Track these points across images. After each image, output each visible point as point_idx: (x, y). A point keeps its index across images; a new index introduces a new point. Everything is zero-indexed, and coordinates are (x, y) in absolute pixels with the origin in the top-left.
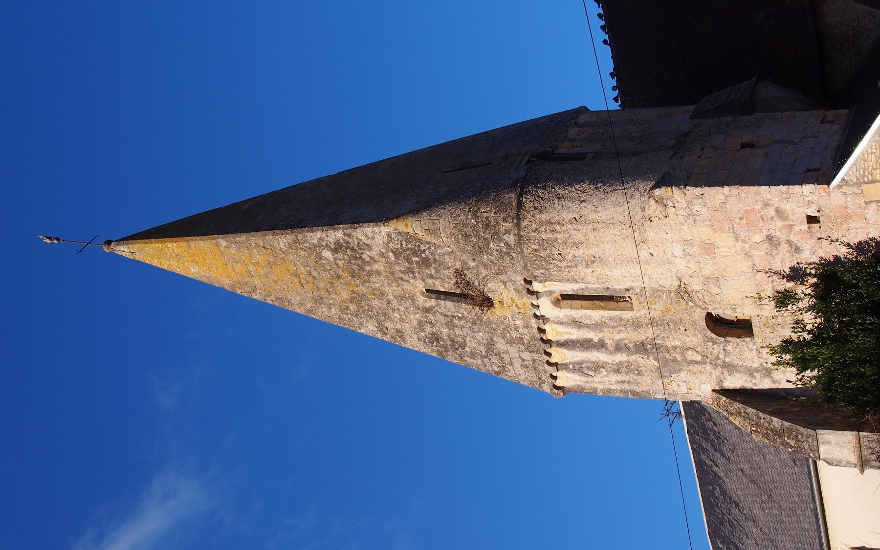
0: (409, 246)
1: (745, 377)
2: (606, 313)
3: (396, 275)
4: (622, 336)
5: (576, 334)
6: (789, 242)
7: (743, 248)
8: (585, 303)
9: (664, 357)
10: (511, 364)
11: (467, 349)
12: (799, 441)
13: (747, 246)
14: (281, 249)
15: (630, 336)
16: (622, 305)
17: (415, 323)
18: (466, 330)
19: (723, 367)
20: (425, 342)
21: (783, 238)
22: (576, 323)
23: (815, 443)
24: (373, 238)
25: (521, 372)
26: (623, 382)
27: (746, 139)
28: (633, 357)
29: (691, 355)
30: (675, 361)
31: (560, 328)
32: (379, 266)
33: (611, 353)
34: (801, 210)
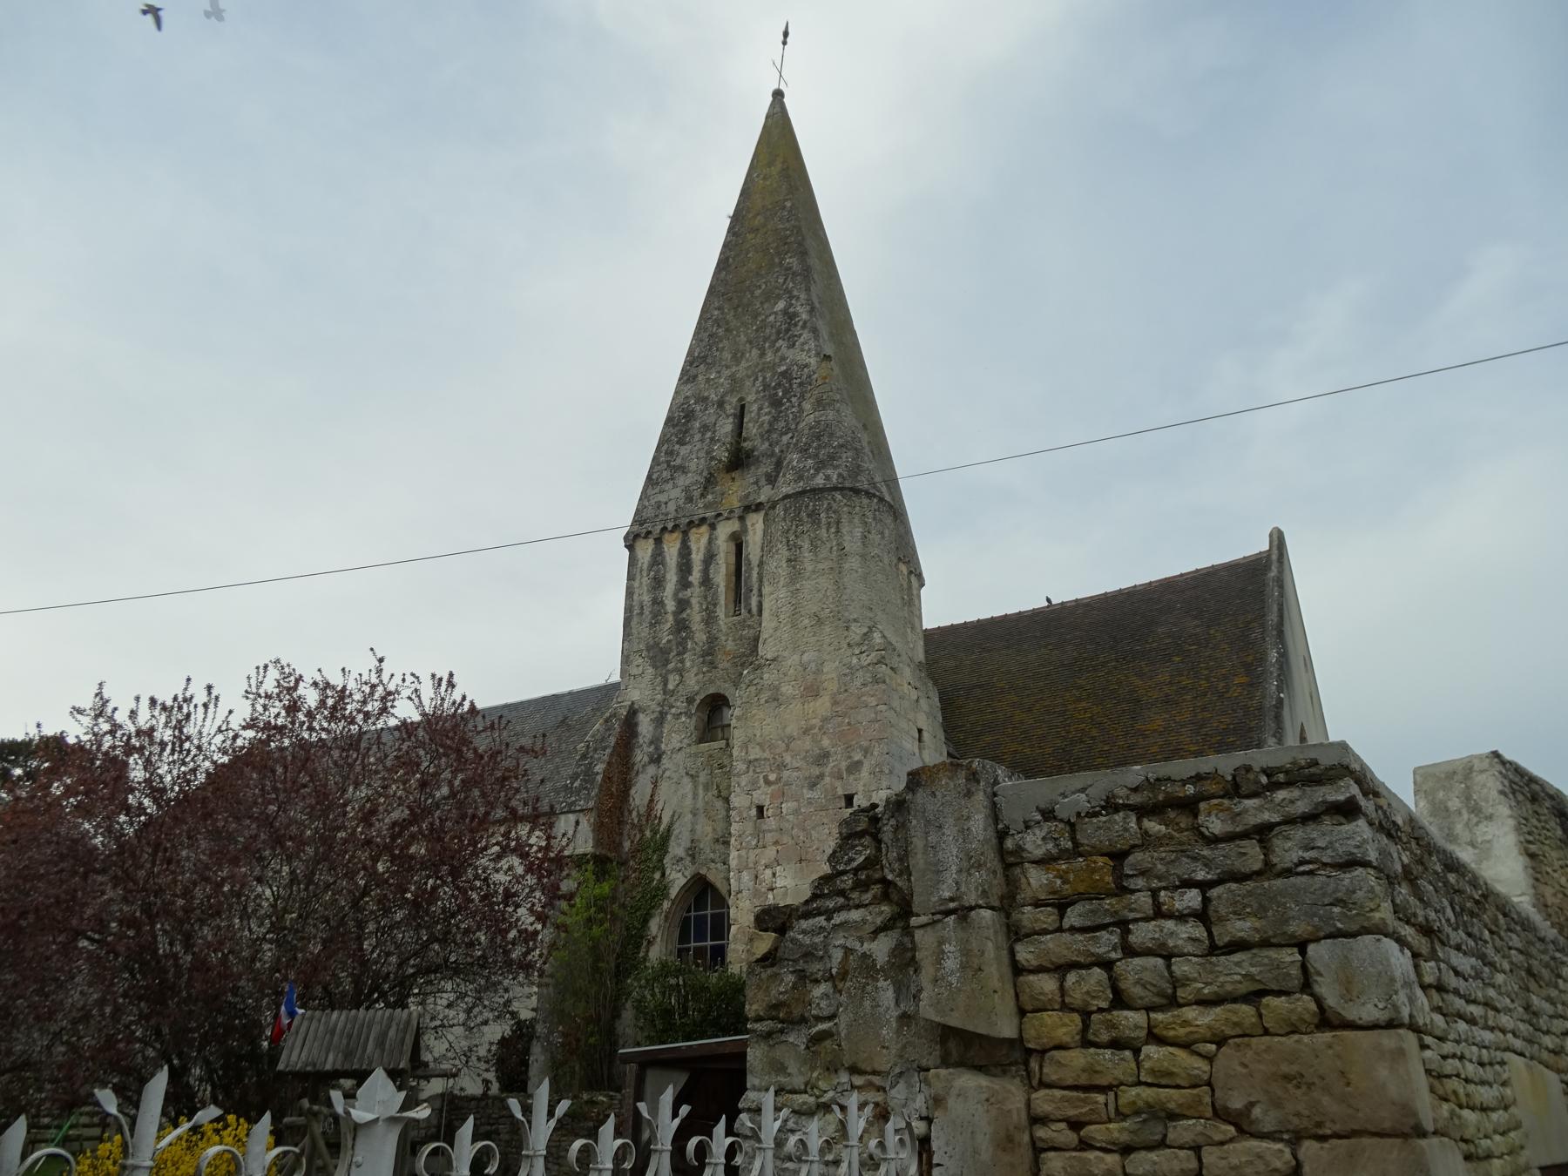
0: (795, 386)
1: (649, 736)
2: (722, 589)
3: (760, 374)
4: (696, 607)
5: (697, 557)
6: (821, 776)
7: (813, 727)
8: (733, 568)
9: (671, 650)
10: (661, 492)
11: (677, 447)
12: (580, 791)
13: (816, 730)
14: (784, 259)
15: (695, 616)
16: (732, 606)
17: (706, 394)
18: (699, 445)
19: (661, 712)
20: (683, 404)
21: (828, 770)
22: (710, 558)
23: (578, 808)
24: (803, 350)
25: (653, 502)
26: (642, 608)
27: (926, 735)
28: (670, 618)
29: (673, 681)
30: (667, 662)
31: (704, 540)
32: (769, 357)
33: (676, 594)
34: (861, 788)
